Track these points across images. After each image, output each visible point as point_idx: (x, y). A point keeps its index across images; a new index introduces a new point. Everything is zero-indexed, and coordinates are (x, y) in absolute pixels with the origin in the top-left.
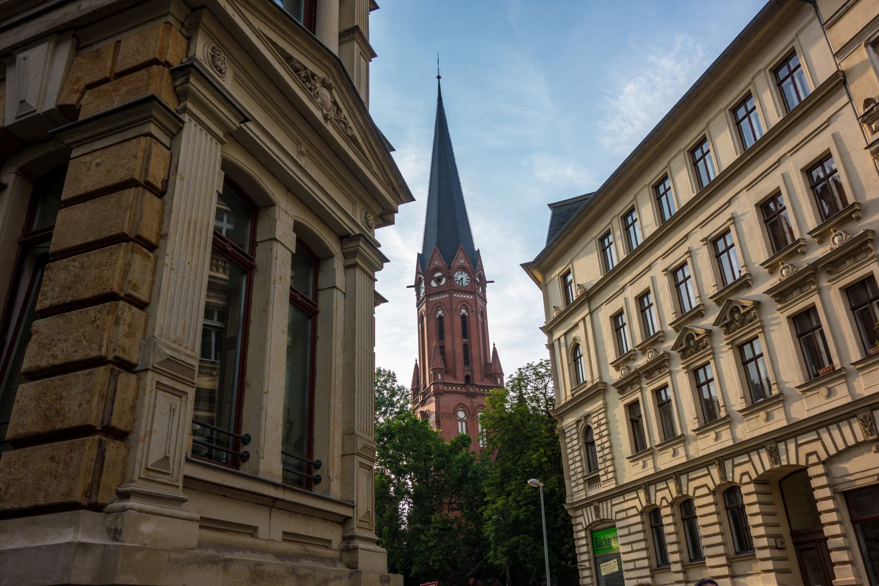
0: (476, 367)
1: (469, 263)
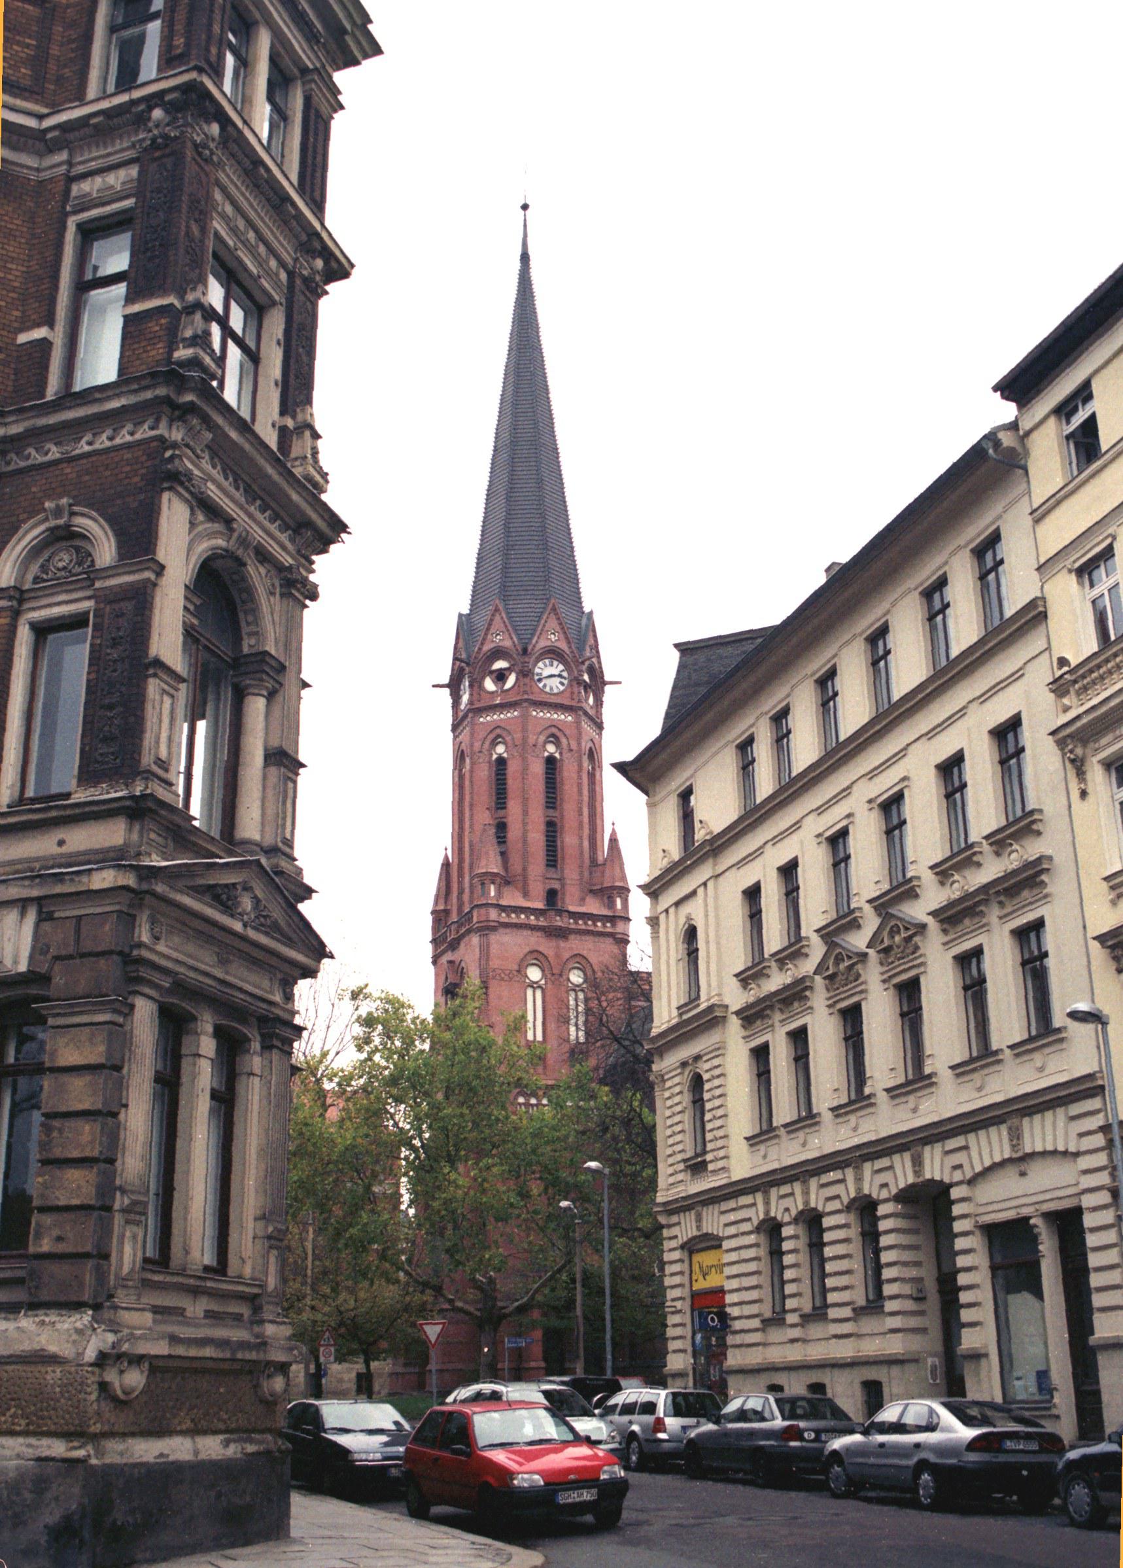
0: (571, 872)
1: (569, 643)
